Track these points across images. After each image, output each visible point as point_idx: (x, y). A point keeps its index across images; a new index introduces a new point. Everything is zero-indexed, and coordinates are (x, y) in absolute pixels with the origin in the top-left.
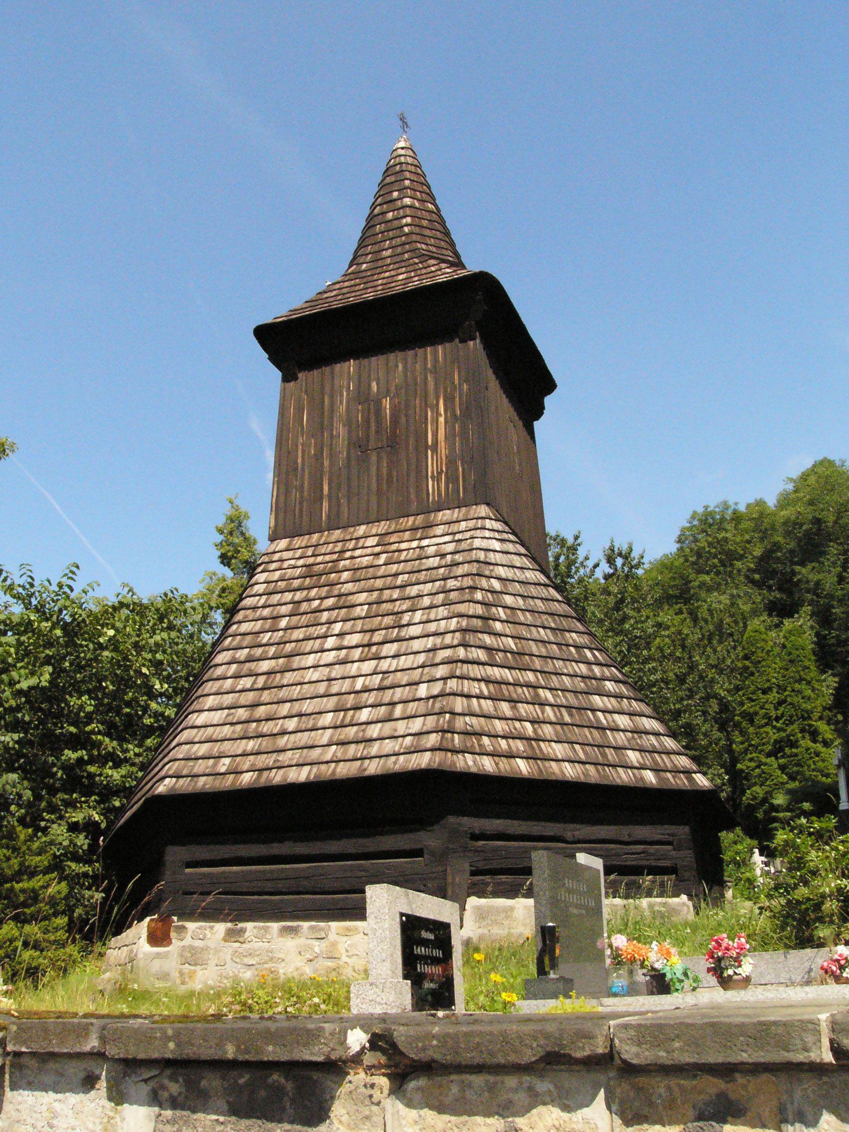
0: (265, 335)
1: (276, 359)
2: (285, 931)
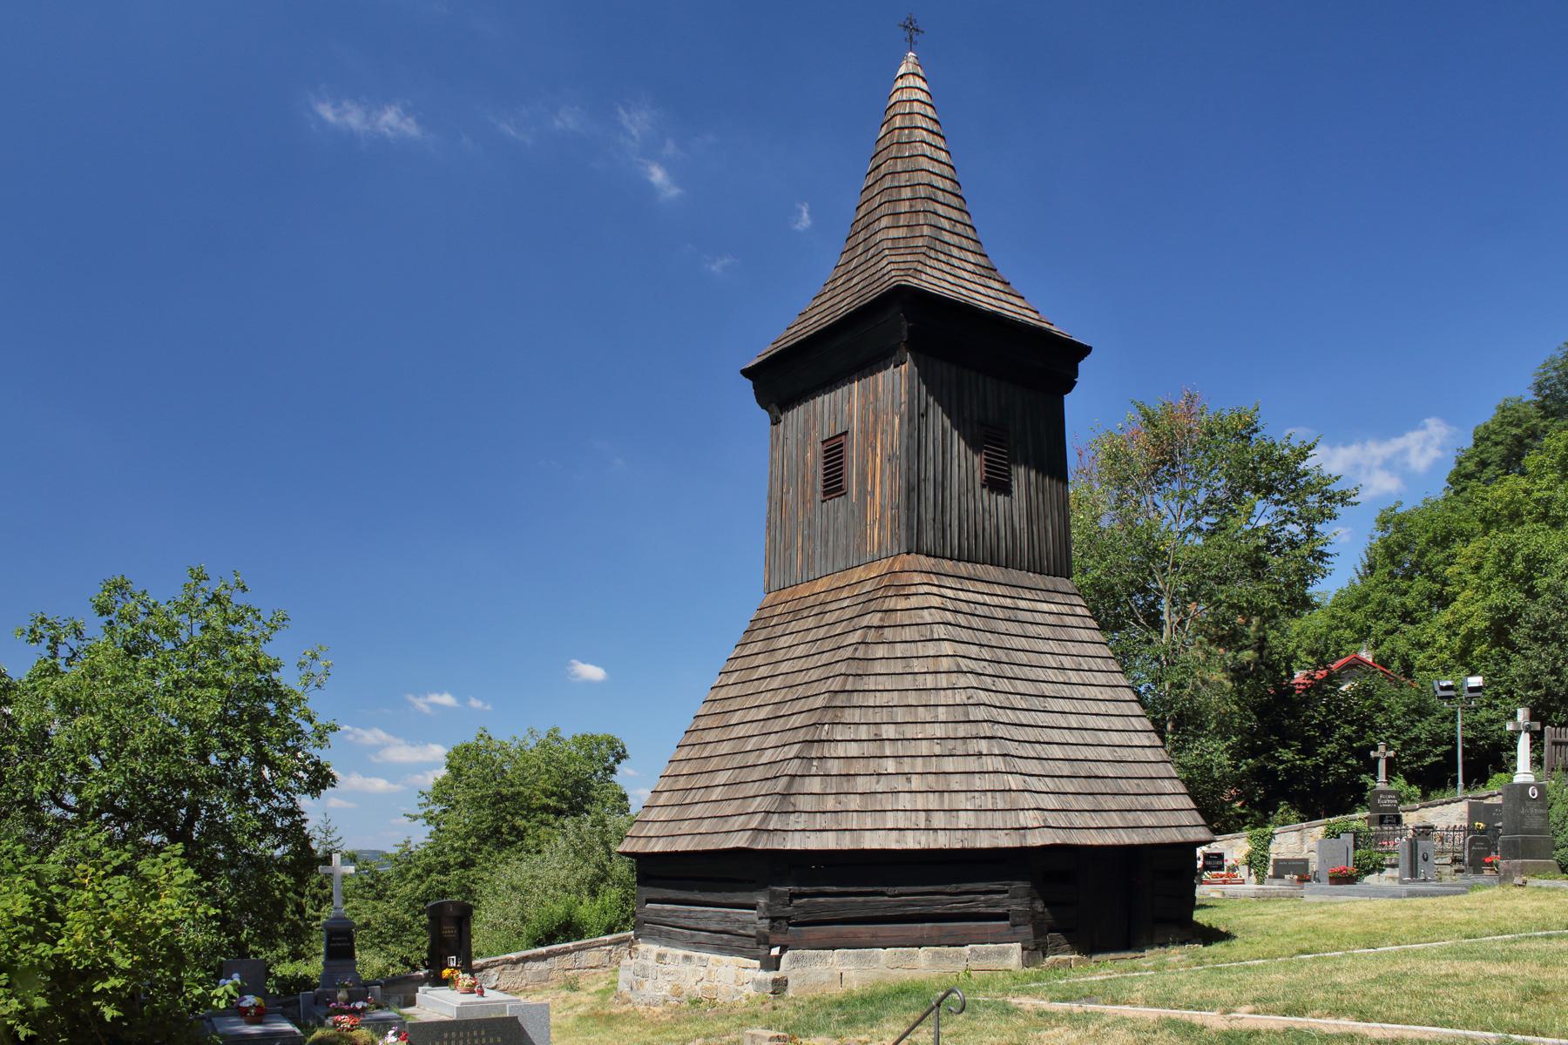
0: (746, 373)
1: (764, 398)
2: (687, 958)
